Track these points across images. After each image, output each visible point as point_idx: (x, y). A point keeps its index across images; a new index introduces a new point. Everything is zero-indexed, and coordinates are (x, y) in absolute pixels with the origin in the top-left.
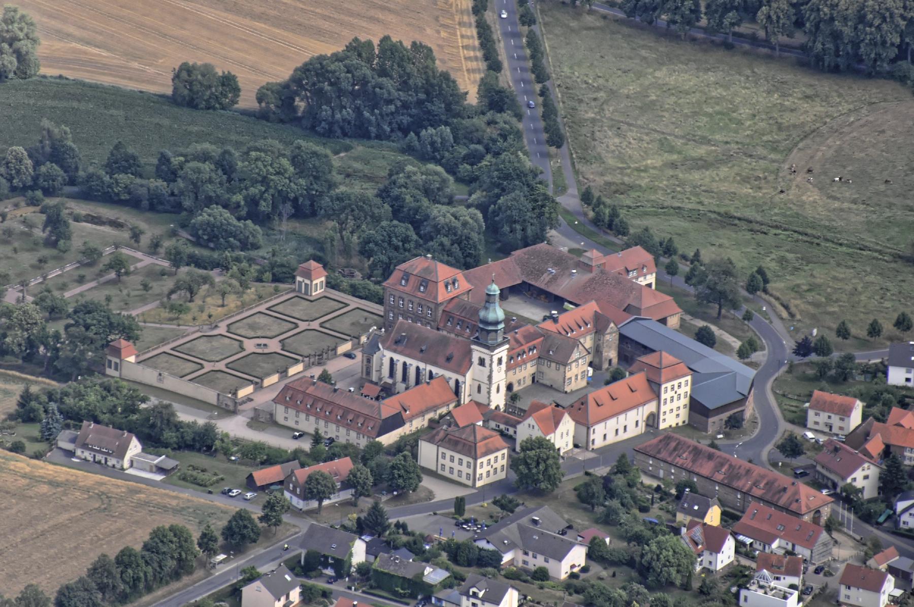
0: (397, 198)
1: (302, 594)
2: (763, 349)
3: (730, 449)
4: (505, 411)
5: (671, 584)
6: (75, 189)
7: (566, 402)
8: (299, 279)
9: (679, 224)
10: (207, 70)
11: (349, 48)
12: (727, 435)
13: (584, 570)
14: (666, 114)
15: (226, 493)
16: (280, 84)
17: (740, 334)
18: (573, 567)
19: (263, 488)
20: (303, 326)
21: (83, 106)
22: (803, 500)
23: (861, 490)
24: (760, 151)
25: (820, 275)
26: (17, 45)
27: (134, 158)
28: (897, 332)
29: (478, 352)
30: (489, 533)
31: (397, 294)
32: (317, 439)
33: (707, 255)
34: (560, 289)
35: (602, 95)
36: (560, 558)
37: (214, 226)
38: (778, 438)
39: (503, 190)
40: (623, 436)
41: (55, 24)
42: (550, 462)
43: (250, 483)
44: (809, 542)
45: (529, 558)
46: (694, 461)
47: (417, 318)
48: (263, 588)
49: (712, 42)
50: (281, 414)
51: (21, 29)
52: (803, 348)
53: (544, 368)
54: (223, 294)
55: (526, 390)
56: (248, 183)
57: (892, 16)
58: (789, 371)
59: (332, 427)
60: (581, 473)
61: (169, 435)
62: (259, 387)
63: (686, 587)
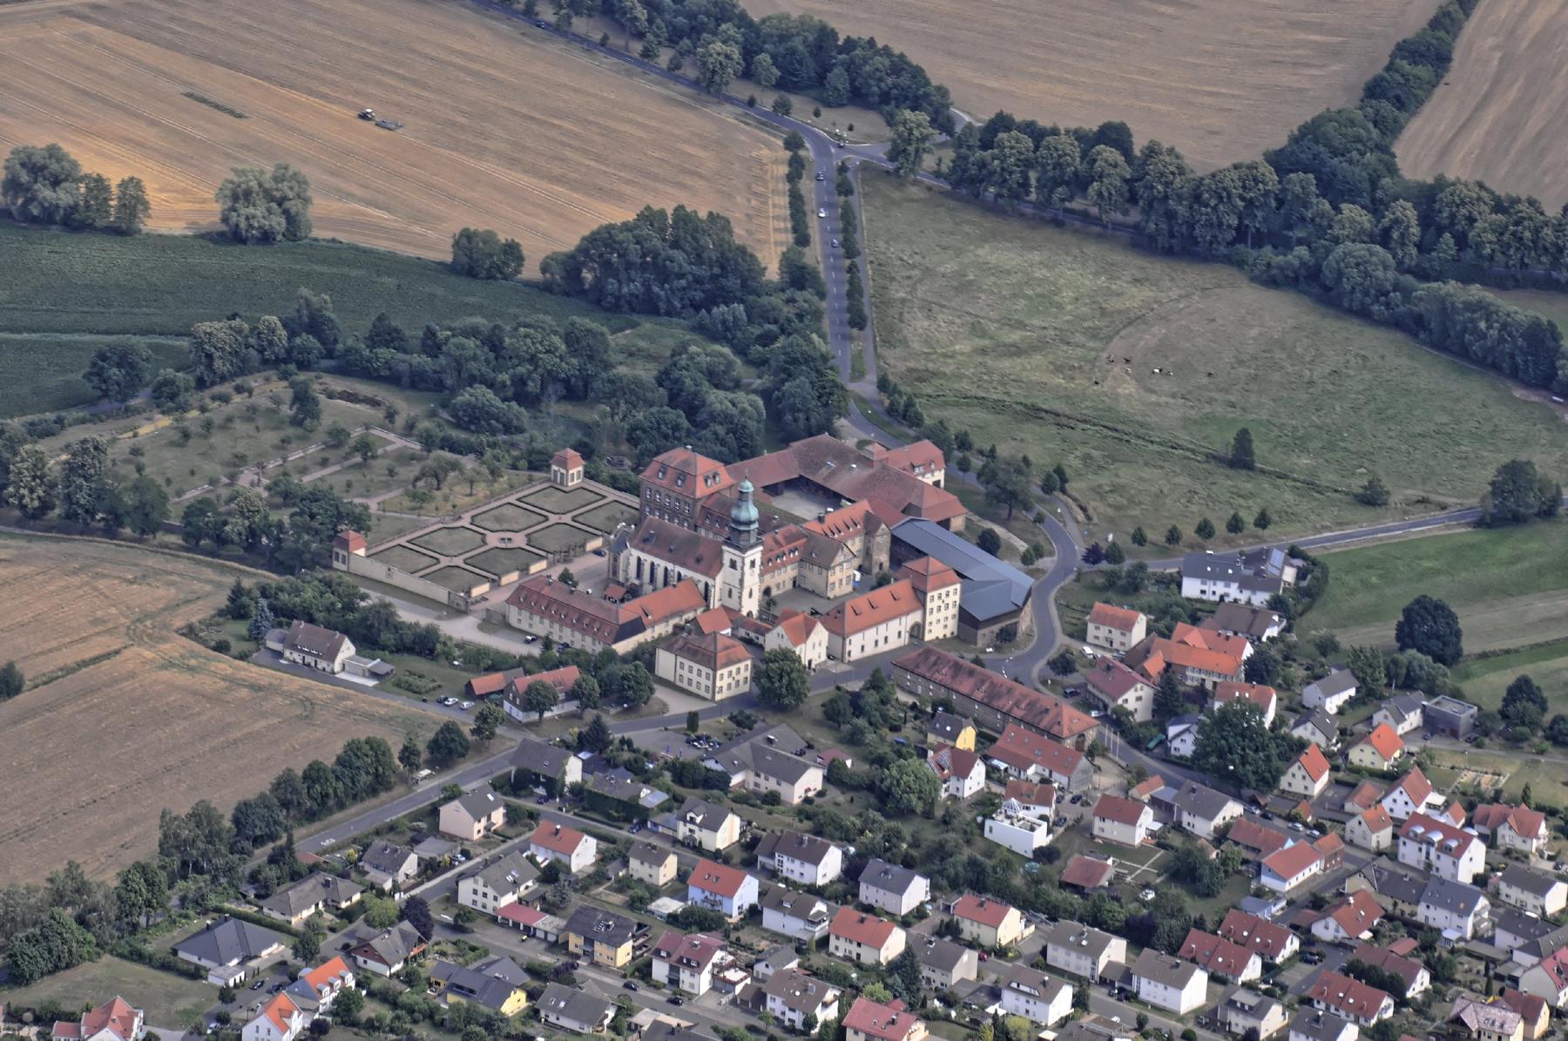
0: (676, 381)
1: (506, 815)
2: (1051, 554)
3: (997, 666)
4: (760, 618)
5: (912, 812)
6: (332, 363)
7: (822, 607)
8: (554, 467)
9: (980, 415)
10: (489, 237)
11: (641, 217)
12: (997, 649)
13: (821, 794)
14: (983, 296)
15: (441, 702)
16: (565, 254)
17: (1030, 537)
18: (808, 790)
19: (482, 697)
20: (553, 519)
21: (354, 273)
22: (1065, 722)
23: (1132, 713)
24: (1079, 338)
25: (1126, 475)
26: (287, 204)
27: (397, 331)
28: (1198, 539)
29: (729, 554)
30: (716, 752)
31: (654, 487)
32: (547, 644)
33: (1003, 451)
34: (835, 486)
35: (916, 273)
36: (793, 781)
37: (474, 407)
38: (1053, 654)
39: (790, 375)
40: (883, 648)
41: (335, 181)
42: (794, 675)
43: (469, 692)
44: (1067, 770)
45: (761, 780)
46: (954, 677)
47: (674, 514)
48: (462, 809)
49: (1042, 219)
50: (515, 616)
51: (291, 188)
52: (1093, 555)
53: (806, 572)
54: (472, 482)
55: (785, 595)
56: (515, 361)
57: (1229, 195)
58: (1078, 580)
59: (567, 631)
60: (832, 688)
61: (387, 637)
62: (495, 584)
63: (928, 815)
